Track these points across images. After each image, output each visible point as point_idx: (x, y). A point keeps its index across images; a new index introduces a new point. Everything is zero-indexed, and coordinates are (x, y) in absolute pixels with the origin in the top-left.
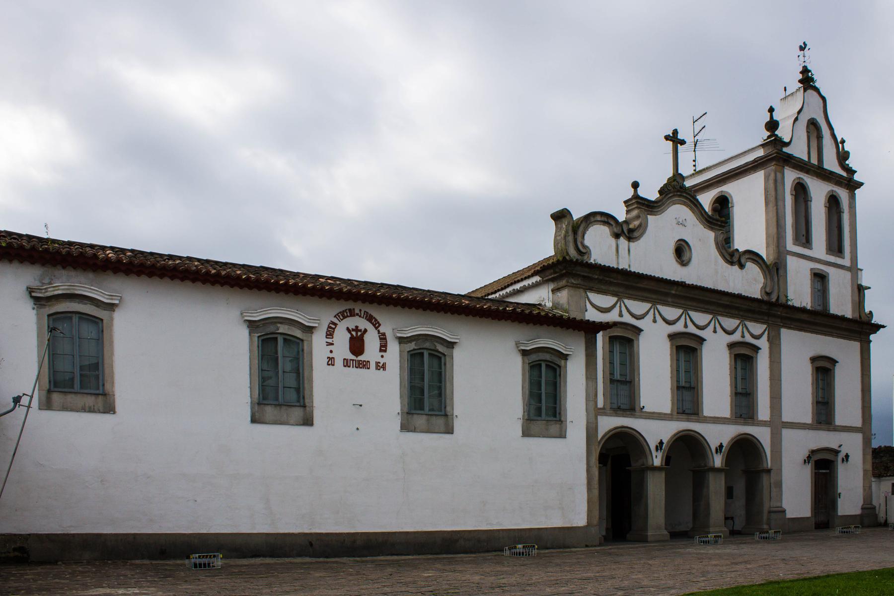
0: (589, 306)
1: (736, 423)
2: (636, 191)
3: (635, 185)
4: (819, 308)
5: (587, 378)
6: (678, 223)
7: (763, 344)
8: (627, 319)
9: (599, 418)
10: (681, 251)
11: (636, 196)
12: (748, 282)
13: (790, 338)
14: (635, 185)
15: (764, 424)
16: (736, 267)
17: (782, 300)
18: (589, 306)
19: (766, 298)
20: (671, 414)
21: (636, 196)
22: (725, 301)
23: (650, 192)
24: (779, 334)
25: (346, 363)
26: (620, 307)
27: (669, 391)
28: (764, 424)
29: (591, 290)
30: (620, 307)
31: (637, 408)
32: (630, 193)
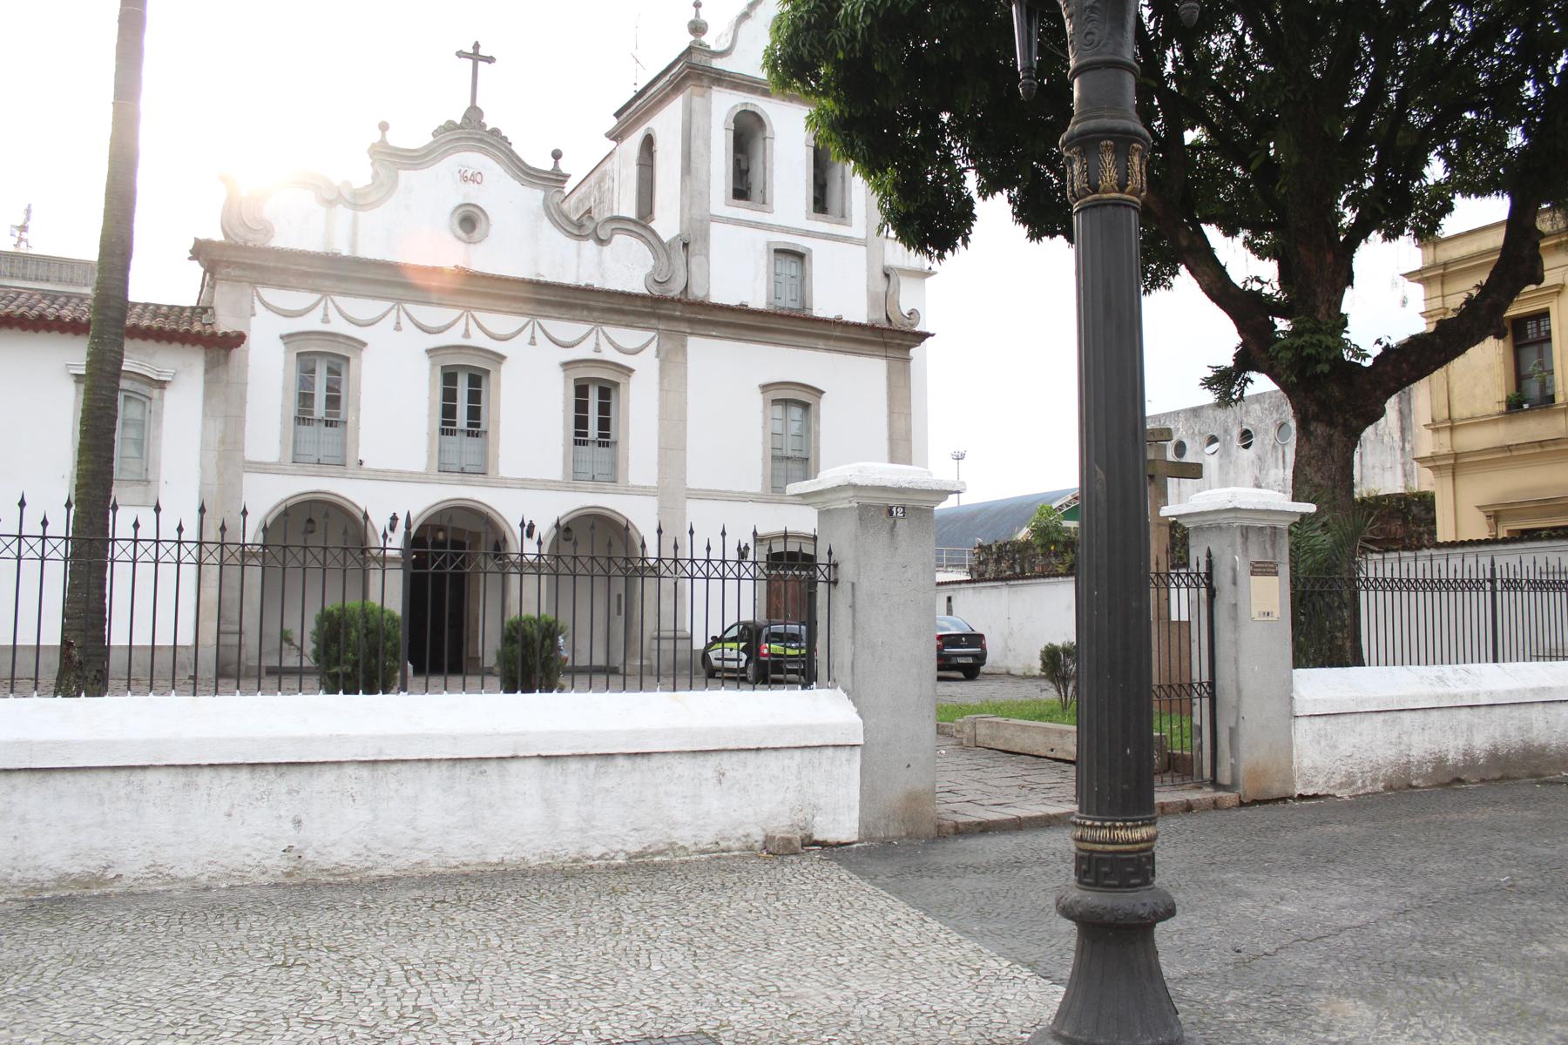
0: (258, 307)
1: (576, 489)
2: (556, 163)
3: (384, 127)
4: (788, 302)
5: (205, 415)
6: (465, 179)
7: (646, 367)
8: (609, 354)
9: (1440, 539)
10: (469, 221)
11: (383, 142)
12: (625, 267)
13: (708, 355)
14: (384, 127)
15: (643, 491)
16: (590, 244)
17: (697, 292)
18: (258, 307)
19: (656, 291)
20: (279, 463)
21: (383, 142)
22: (370, 274)
23: (416, 136)
24: (684, 346)
25: (469, 434)
26: (326, 308)
27: (760, 464)
28: (643, 491)
29: (265, 284)
30: (326, 308)
31: (351, 462)
32: (376, 136)
